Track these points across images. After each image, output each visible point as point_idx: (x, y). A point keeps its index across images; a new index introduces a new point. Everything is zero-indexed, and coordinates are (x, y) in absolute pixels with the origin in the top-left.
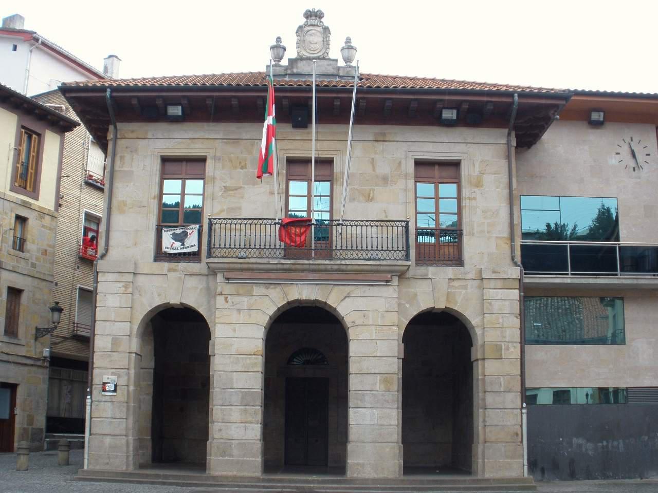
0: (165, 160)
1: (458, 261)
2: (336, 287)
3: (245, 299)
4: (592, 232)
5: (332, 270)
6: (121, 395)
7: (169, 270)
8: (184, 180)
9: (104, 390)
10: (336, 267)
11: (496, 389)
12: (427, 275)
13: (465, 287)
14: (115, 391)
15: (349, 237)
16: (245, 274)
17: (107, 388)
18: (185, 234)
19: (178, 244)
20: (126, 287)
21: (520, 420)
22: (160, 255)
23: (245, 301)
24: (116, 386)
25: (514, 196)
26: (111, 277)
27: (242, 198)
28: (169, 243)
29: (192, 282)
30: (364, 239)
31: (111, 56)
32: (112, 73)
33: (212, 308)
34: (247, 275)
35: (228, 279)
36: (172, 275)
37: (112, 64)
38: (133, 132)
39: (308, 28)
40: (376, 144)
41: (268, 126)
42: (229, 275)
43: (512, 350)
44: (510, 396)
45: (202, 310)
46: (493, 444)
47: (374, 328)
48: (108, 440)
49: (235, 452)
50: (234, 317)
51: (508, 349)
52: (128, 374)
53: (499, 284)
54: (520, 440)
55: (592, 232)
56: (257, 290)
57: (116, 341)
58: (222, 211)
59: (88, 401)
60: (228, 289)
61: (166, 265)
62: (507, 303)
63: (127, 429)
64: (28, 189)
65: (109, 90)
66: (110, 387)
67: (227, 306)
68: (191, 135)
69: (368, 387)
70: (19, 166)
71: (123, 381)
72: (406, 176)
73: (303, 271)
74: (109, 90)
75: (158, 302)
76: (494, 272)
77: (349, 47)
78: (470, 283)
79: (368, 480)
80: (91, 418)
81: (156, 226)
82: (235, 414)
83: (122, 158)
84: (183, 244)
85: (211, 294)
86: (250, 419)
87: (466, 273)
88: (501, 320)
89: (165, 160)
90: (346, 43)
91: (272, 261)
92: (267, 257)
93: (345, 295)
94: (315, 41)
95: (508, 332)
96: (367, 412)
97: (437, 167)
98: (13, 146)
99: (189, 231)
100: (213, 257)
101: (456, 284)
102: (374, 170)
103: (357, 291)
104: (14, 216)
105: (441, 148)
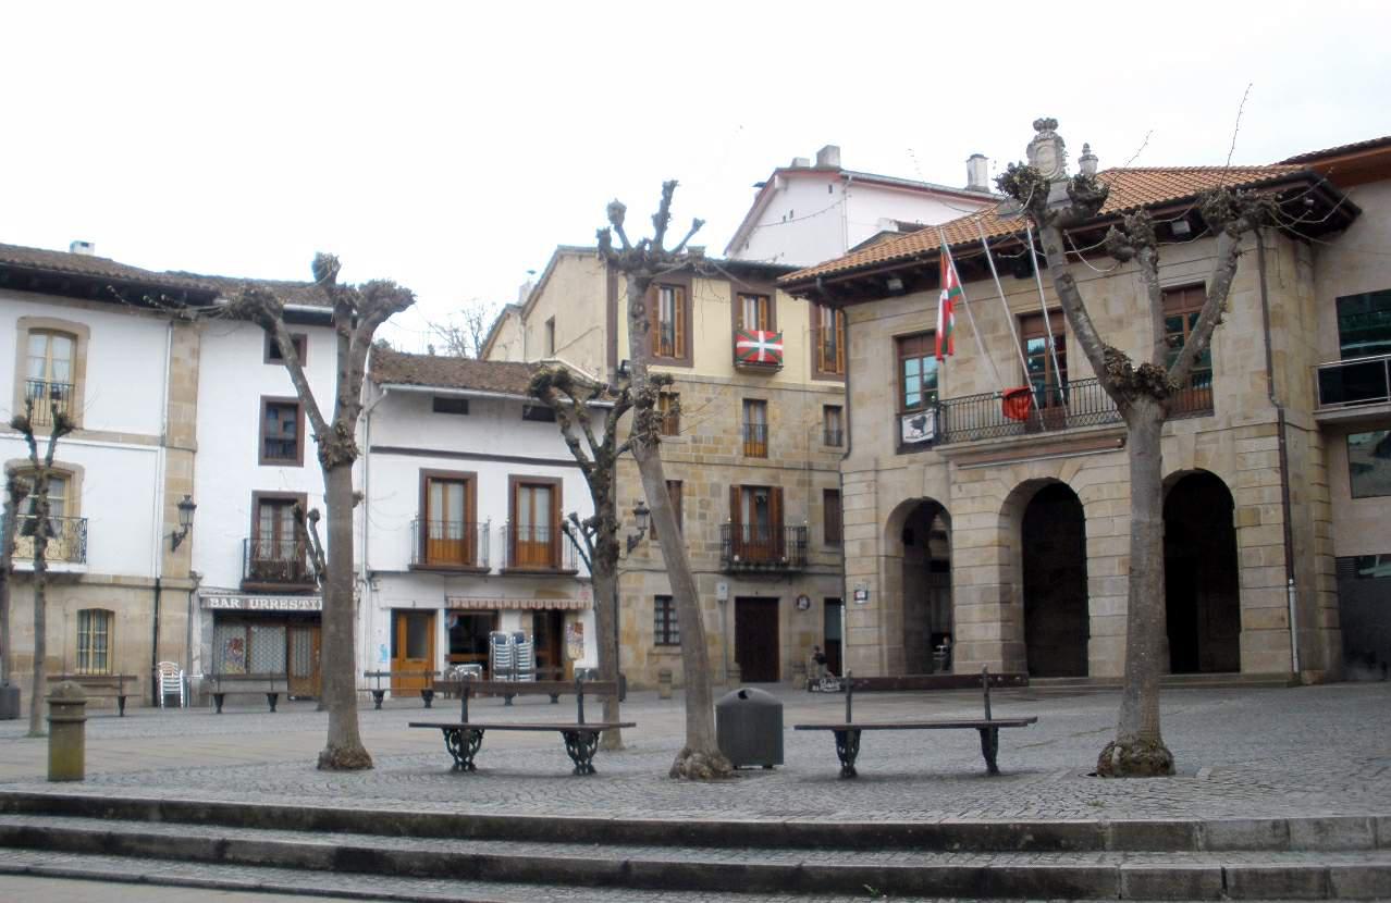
0: (900, 340)
1: (1208, 409)
2: (1068, 461)
3: (977, 485)
4: (1134, 396)
5: (1059, 442)
6: (873, 603)
7: (911, 462)
8: (921, 358)
9: (856, 599)
10: (1062, 438)
11: (1254, 563)
12: (1170, 432)
13: (1216, 441)
14: (866, 598)
15: (1088, 397)
16: (976, 458)
17: (859, 596)
18: (924, 420)
19: (918, 432)
20: (869, 486)
21: (1285, 599)
22: (903, 448)
23: (977, 488)
24: (867, 593)
25: (1270, 314)
26: (855, 477)
27: (974, 370)
28: (911, 434)
29: (932, 472)
30: (1078, 403)
31: (973, 157)
32: (977, 179)
33: (950, 500)
34: (976, 459)
35: (960, 465)
36: (913, 467)
37: (975, 167)
38: (861, 314)
39: (1039, 145)
40: (1107, 280)
41: (944, 301)
42: (961, 461)
43: (1272, 512)
44: (1272, 571)
45: (943, 503)
46: (1255, 632)
47: (1108, 503)
48: (862, 651)
49: (977, 655)
50: (969, 506)
51: (1267, 512)
52: (878, 581)
53: (1253, 431)
54: (1287, 625)
55: (1134, 396)
56: (990, 474)
57: (863, 546)
58: (955, 389)
59: (843, 611)
60: (960, 476)
61: (906, 458)
62: (1264, 455)
63: (880, 637)
64: (838, 371)
65: (818, 279)
66: (861, 595)
67: (960, 496)
68: (918, 307)
69: (1107, 572)
70: (821, 348)
71: (872, 587)
72: (1143, 314)
73: (1031, 446)
74: (818, 279)
75: (902, 499)
76: (1246, 418)
77: (1087, 157)
78: (1222, 434)
79: (1105, 679)
80: (846, 629)
81: (1156, 343)
82: (976, 612)
83: (856, 346)
84: (922, 432)
85: (949, 482)
86: (990, 617)
87: (1216, 423)
88: (1257, 478)
89: (900, 340)
90: (1084, 152)
91: (1008, 439)
92: (992, 437)
93: (1076, 468)
94: (1047, 160)
95: (1267, 492)
96: (1106, 601)
97: (1183, 294)
98: (807, 327)
99: (927, 416)
100: (953, 442)
101: (1205, 438)
102: (1107, 313)
103: (1089, 462)
104: (821, 407)
105: (1183, 269)
